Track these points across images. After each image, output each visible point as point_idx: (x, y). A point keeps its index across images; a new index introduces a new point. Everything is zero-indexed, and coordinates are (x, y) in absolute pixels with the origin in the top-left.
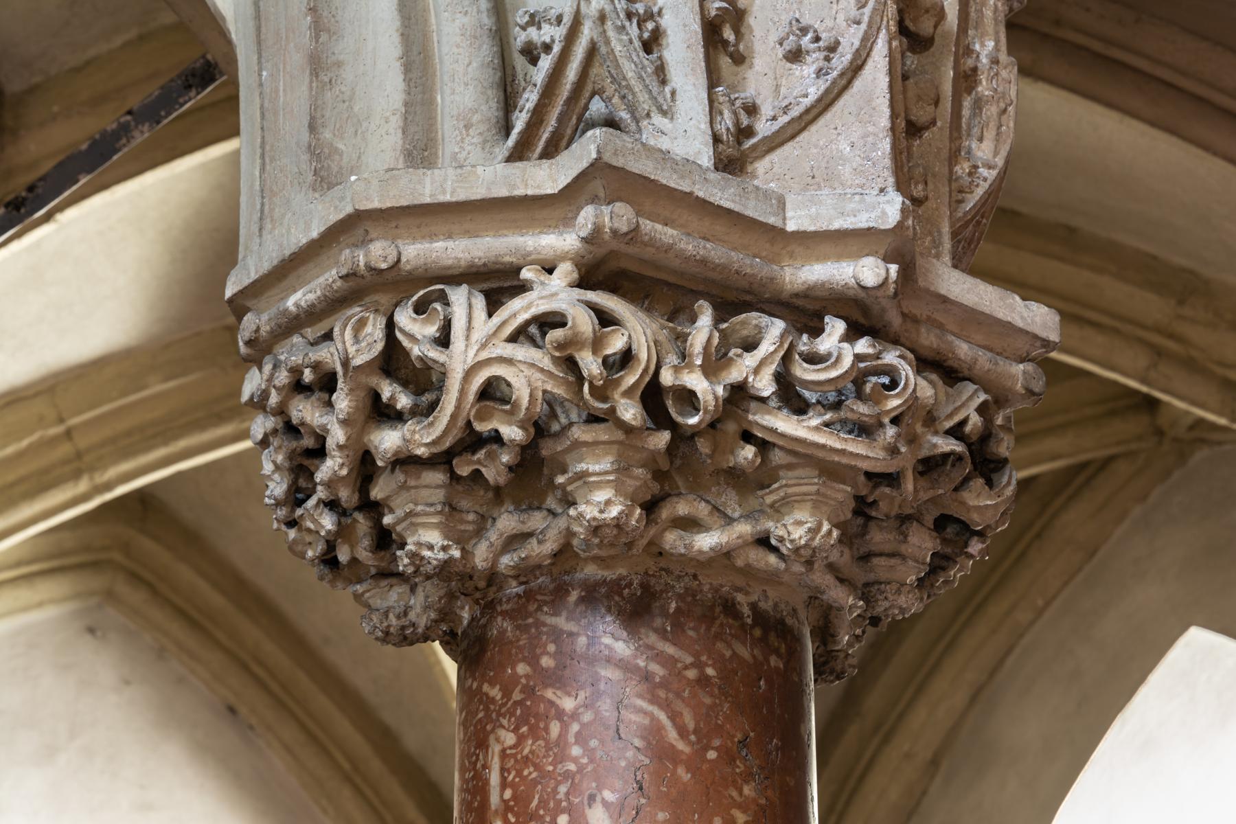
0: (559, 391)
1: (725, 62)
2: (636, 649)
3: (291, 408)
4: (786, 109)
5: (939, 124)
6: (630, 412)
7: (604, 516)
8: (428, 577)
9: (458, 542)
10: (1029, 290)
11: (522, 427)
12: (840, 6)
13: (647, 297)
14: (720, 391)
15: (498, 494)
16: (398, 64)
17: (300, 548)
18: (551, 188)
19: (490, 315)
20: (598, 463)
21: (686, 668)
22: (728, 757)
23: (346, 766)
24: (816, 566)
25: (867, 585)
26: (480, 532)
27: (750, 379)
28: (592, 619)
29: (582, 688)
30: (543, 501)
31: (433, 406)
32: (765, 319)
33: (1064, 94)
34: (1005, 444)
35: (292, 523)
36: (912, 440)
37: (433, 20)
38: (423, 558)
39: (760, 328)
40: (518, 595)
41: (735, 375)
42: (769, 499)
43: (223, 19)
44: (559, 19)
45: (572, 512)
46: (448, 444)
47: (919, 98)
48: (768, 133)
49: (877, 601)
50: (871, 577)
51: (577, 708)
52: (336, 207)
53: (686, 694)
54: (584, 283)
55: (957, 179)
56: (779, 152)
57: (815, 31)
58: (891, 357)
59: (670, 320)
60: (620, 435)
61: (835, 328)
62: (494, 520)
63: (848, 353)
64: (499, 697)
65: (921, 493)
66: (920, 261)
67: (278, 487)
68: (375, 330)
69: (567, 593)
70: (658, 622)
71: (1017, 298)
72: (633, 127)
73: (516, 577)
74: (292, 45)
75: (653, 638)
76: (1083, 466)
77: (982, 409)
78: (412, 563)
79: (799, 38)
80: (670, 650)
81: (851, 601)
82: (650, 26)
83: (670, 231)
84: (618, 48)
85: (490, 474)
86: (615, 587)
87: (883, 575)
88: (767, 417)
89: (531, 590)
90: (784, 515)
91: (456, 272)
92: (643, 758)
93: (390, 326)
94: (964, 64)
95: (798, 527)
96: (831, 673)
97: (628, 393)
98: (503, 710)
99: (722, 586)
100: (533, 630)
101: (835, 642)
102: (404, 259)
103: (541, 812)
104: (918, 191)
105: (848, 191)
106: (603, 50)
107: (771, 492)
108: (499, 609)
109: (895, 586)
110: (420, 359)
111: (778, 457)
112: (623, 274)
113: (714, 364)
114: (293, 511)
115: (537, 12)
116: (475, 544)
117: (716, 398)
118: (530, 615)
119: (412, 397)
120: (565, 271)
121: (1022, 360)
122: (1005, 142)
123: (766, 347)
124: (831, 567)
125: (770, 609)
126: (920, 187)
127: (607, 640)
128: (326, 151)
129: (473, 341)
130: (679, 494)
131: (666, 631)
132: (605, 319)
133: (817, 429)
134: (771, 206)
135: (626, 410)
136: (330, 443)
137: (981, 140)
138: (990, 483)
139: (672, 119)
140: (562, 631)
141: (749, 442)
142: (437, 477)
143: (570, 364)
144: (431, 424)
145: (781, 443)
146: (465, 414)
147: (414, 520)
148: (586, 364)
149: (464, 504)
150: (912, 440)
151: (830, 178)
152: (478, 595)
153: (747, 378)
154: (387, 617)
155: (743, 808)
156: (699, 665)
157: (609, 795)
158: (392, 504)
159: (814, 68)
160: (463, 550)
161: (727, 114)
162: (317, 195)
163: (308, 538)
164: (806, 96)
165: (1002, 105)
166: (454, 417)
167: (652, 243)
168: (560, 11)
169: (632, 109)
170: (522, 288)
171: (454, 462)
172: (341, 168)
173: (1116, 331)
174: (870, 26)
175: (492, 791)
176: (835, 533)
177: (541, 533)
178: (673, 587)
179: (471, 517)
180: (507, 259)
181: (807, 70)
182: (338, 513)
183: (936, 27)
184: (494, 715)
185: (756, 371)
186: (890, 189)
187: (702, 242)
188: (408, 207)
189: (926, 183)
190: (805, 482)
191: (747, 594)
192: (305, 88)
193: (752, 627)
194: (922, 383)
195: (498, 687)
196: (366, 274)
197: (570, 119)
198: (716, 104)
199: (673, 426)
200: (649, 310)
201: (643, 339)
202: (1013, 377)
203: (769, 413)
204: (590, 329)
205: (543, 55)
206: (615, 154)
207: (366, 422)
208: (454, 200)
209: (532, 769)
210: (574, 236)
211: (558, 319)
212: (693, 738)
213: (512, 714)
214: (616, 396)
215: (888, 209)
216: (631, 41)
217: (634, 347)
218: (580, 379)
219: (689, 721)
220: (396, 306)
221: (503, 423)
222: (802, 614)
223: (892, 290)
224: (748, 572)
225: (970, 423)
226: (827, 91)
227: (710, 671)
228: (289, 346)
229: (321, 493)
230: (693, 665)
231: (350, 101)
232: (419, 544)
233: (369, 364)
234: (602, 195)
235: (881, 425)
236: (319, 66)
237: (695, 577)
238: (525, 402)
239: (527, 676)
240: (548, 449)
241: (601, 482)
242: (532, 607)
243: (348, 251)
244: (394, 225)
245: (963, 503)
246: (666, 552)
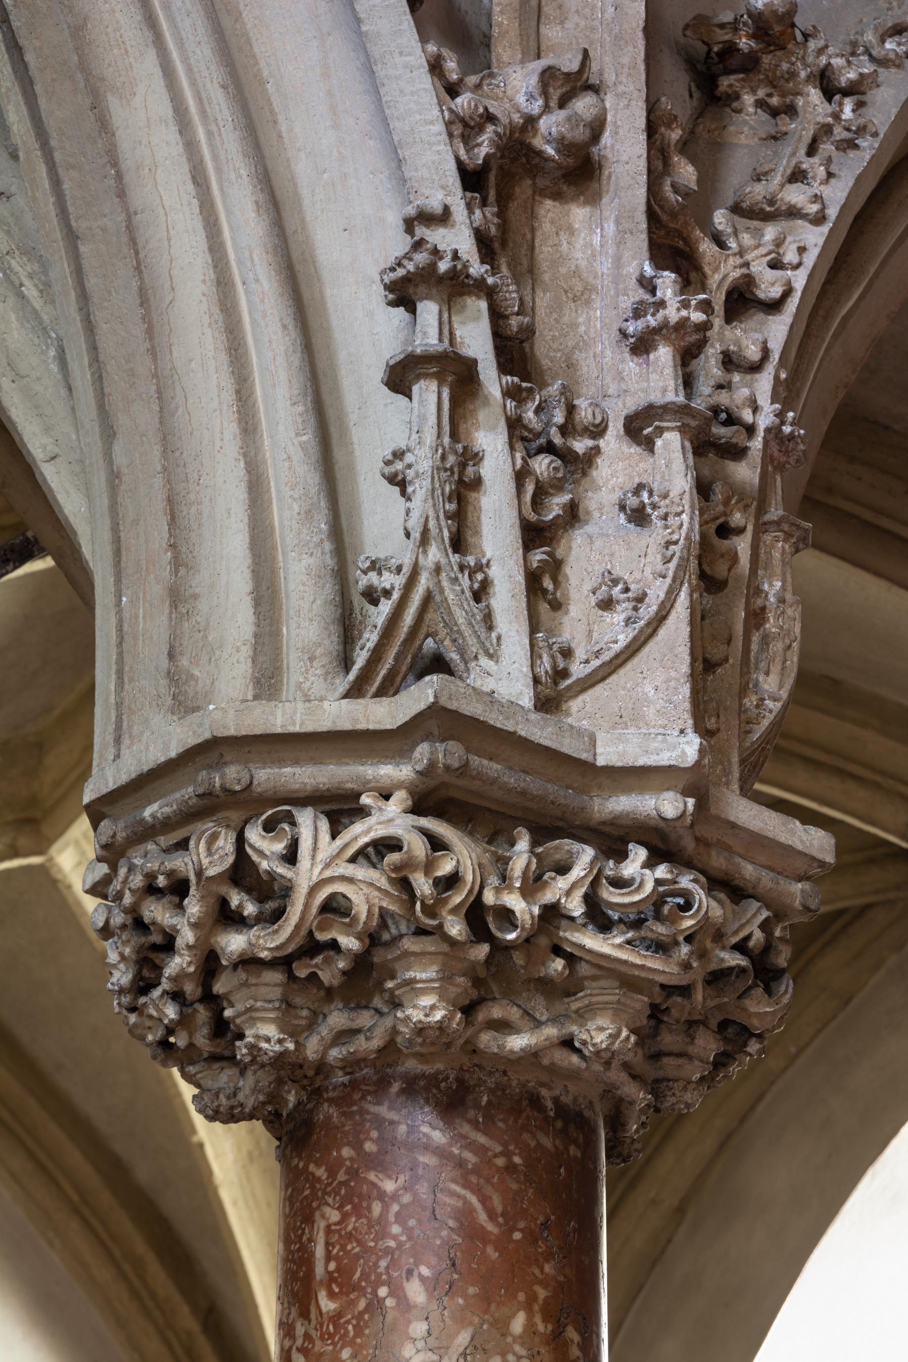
0: (393, 907)
1: (544, 607)
2: (452, 1138)
3: (143, 908)
4: (597, 654)
5: (731, 661)
6: (456, 928)
7: (429, 1019)
8: (263, 1066)
9: (291, 1035)
10: (808, 818)
11: (359, 938)
12: (648, 560)
13: (470, 821)
14: (536, 911)
15: (330, 993)
16: (249, 598)
17: (139, 1031)
18: (390, 724)
19: (334, 837)
20: (424, 971)
21: (496, 1156)
22: (532, 1238)
23: (75, 1197)
24: (613, 1065)
25: (657, 1081)
26: (311, 1026)
27: (563, 901)
28: (411, 1109)
29: (401, 1172)
30: (370, 1000)
31: (278, 915)
32: (576, 846)
33: (834, 561)
34: (784, 956)
35: (133, 1009)
36: (702, 955)
37: (280, 558)
38: (260, 1049)
39: (572, 853)
40: (343, 1084)
41: (549, 896)
42: (574, 1006)
43: (75, 533)
44: (399, 569)
45: (399, 1014)
46: (290, 950)
47: (714, 638)
48: (581, 675)
49: (665, 1096)
50: (661, 1074)
51: (397, 1191)
52: (194, 732)
53: (495, 1180)
54: (417, 809)
55: (745, 711)
56: (590, 692)
57: (625, 583)
58: (685, 881)
59: (489, 842)
60: (445, 947)
61: (638, 854)
62: (325, 1016)
63: (649, 879)
64: (324, 1177)
65: (709, 1001)
66: (713, 791)
67: (122, 977)
68: (226, 843)
69: (390, 1084)
70: (471, 1113)
71: (798, 823)
72: (462, 667)
73: (342, 1068)
74: (152, 576)
75: (466, 1129)
76: (841, 913)
77: (765, 926)
78: (250, 1054)
79: (611, 588)
80: (482, 1139)
81: (641, 1095)
82: (479, 577)
83: (496, 766)
84: (451, 597)
85: (325, 977)
86: (434, 1080)
87: (671, 1073)
88: (576, 934)
89: (356, 1080)
90: (587, 1020)
91: (301, 795)
92: (456, 1237)
93: (241, 841)
94: (754, 603)
95: (599, 1032)
96: (618, 1156)
97: (454, 911)
98: (329, 1189)
99: (528, 1081)
100: (357, 1117)
101: (624, 1131)
102: (255, 782)
103: (363, 1284)
104: (711, 724)
105: (652, 730)
106: (438, 598)
107: (576, 1000)
108: (325, 1096)
109: (682, 1084)
110: (268, 873)
111: (584, 969)
112: (451, 801)
113: (532, 885)
114: (136, 998)
115: (378, 559)
116: (307, 1037)
117: (532, 917)
118: (355, 1104)
119: (258, 905)
120: (400, 798)
121: (800, 880)
122: (789, 676)
123: (577, 872)
124: (626, 1066)
125: (569, 1103)
126: (713, 720)
127: (425, 1129)
128: (184, 677)
129: (316, 860)
130: (494, 999)
131: (478, 1122)
132: (437, 844)
133: (620, 946)
134: (584, 743)
135: (452, 926)
136: (180, 942)
137: (767, 673)
138: (768, 991)
139: (497, 662)
140: (384, 1120)
141: (558, 955)
142: (276, 977)
143: (405, 885)
144: (276, 932)
145: (588, 958)
146: (307, 925)
147: (254, 1014)
148: (419, 885)
149: (298, 1000)
150: (702, 955)
151: (637, 718)
152: (305, 1082)
153: (559, 899)
154: (218, 1097)
155: (544, 1284)
156: (507, 1154)
157: (425, 1271)
158: (232, 999)
159: (623, 617)
160: (297, 1043)
161: (545, 658)
162: (175, 718)
163: (148, 1023)
164: (616, 642)
165: (787, 641)
166: (298, 927)
167: (479, 776)
168: (400, 562)
169: (462, 652)
170: (363, 812)
171: (294, 965)
172: (196, 693)
173: (878, 786)
174: (674, 580)
175: (317, 1263)
176: (633, 1039)
177: (369, 1030)
178: (485, 1082)
179: (305, 1013)
180: (349, 786)
181: (617, 617)
182: (179, 1003)
183: (729, 570)
184: (320, 1194)
185: (568, 893)
186: (689, 731)
187: (523, 775)
188: (261, 736)
189: (718, 716)
190: (605, 992)
191: (550, 1089)
192: (164, 618)
193: (555, 1119)
194: (714, 904)
195: (324, 1168)
196: (221, 794)
197: (405, 658)
198: (536, 648)
199: (489, 938)
200: (471, 834)
201: (469, 863)
202: (792, 895)
203: (578, 931)
204: (424, 854)
205: (382, 599)
206: (450, 698)
207: (214, 925)
208: (303, 731)
209: (355, 1244)
210: (410, 768)
211: (394, 842)
212: (501, 1220)
213: (337, 1193)
214: (444, 913)
215: (687, 749)
216: (463, 592)
217: (461, 869)
218: (412, 897)
219: (497, 1203)
220: (246, 822)
221: (341, 933)
222: (598, 1107)
223: (689, 821)
224: (553, 1070)
225: (754, 938)
226: (635, 639)
227: (517, 1160)
228: (142, 852)
229: (165, 985)
230: (502, 1154)
231: (205, 630)
232: (257, 1037)
233: (220, 875)
234: (436, 733)
235: (676, 943)
236: (178, 598)
237: (505, 1073)
238: (363, 917)
239: (351, 1159)
240: (378, 957)
241: (426, 988)
242: (357, 1096)
243: (204, 772)
244: (247, 750)
245: (745, 1010)
246: (480, 1050)
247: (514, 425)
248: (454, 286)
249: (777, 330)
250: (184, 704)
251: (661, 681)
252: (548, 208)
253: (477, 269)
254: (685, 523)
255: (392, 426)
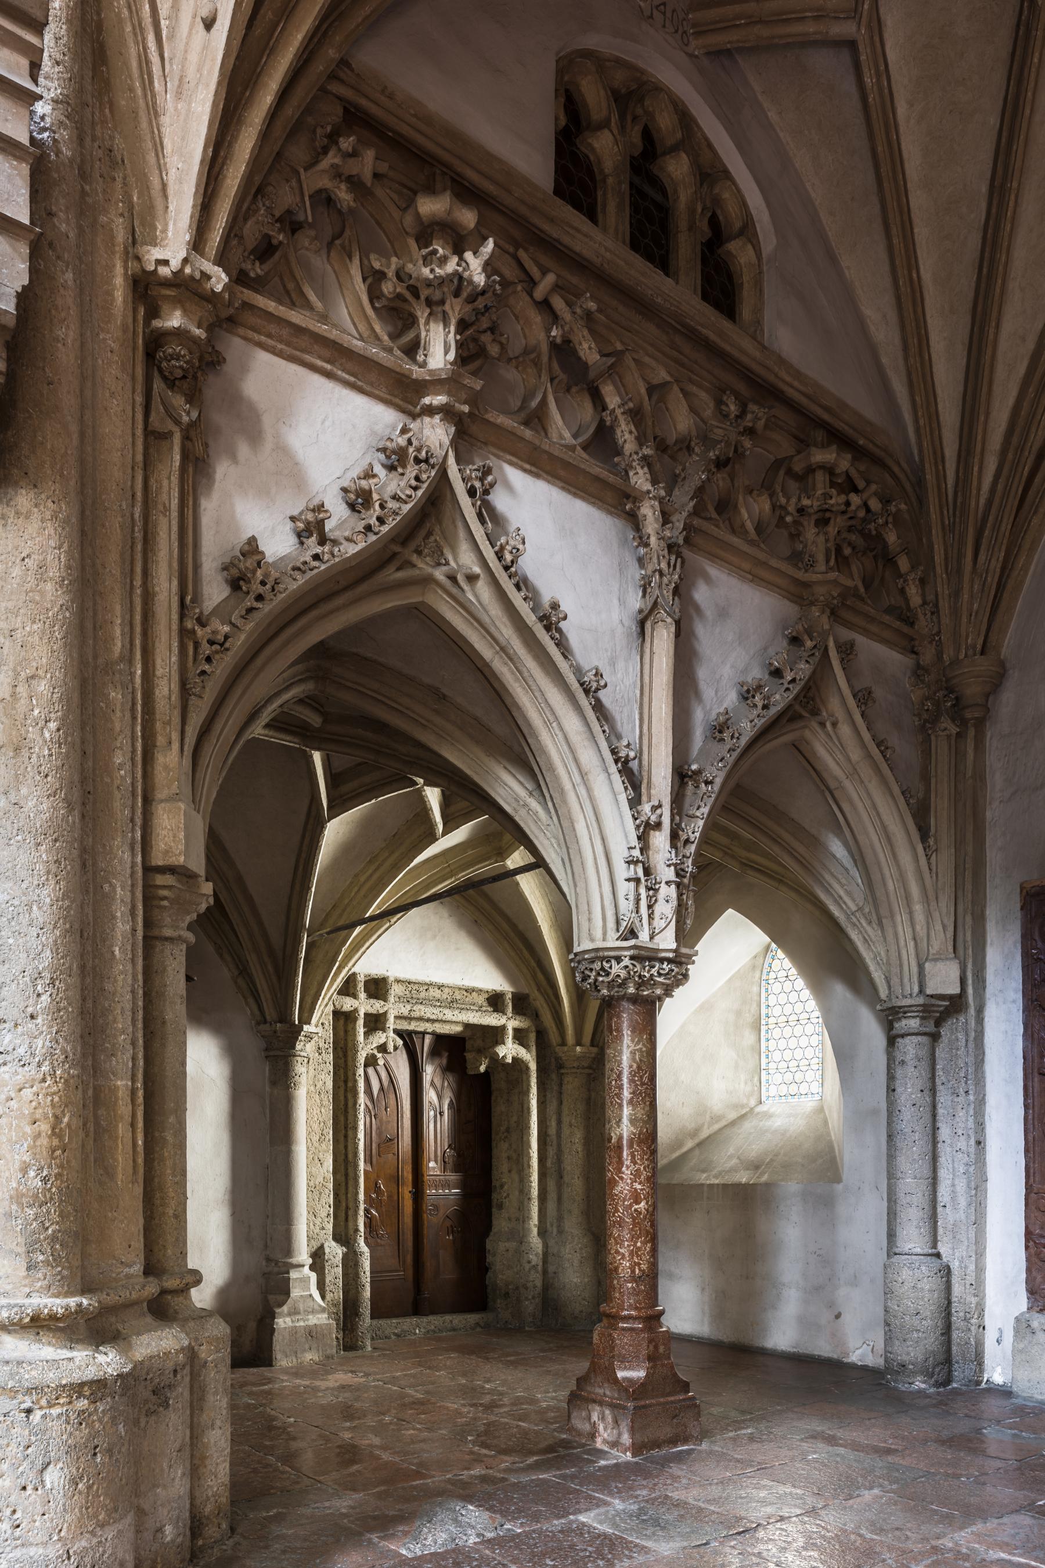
61: (666, 963)
113: (649, 971)
129: (616, 969)
215: (674, 946)
236: (589, 920)
247: (646, 887)
248: (636, 862)
249: (692, 848)
250: (592, 940)
251: (670, 933)
252: (652, 832)
253: (641, 858)
254: (675, 903)
255: (625, 888)
